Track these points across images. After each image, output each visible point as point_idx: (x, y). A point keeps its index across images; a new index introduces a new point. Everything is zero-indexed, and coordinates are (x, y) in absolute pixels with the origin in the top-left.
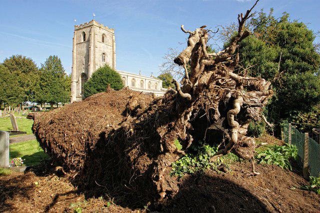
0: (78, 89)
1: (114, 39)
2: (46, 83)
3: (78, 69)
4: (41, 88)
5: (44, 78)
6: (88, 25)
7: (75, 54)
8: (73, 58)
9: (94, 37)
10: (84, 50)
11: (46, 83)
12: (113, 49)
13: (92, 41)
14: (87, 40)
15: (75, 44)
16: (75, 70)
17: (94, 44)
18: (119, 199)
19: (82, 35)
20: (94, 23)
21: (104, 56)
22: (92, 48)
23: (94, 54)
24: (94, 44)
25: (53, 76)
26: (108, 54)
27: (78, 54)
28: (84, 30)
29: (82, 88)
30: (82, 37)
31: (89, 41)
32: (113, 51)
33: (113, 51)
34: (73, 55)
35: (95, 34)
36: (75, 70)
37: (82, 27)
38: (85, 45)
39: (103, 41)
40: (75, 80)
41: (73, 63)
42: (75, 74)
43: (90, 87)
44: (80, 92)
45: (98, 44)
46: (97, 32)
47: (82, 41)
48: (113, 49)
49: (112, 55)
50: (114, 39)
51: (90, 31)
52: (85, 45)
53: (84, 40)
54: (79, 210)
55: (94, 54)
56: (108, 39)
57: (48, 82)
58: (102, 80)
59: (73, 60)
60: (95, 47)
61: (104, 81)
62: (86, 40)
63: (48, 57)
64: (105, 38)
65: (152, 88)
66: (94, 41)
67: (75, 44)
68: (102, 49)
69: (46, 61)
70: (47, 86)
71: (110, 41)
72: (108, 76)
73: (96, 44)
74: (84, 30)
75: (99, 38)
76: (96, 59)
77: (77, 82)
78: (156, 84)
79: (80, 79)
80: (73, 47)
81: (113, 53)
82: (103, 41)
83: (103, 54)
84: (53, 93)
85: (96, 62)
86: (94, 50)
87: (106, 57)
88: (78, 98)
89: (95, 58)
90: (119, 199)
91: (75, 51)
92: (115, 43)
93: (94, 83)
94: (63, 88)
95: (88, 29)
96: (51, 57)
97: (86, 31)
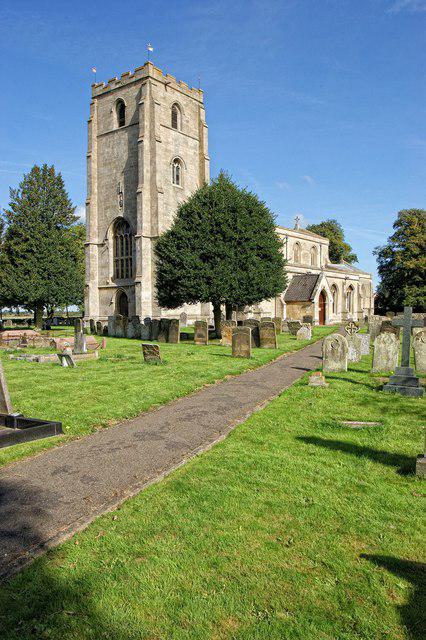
0: (104, 266)
1: (203, 118)
2: (24, 246)
3: (104, 206)
4: (13, 262)
5: (21, 231)
6: (134, 79)
7: (94, 166)
8: (90, 176)
9: (152, 113)
10: (122, 152)
11: (24, 246)
12: (201, 147)
13: (147, 123)
14: (130, 123)
15: (94, 136)
16: (95, 209)
17: (152, 131)
18: (31, 555)
19: (114, 111)
20: (152, 72)
21: (178, 168)
22: (146, 143)
23: (153, 162)
24: (152, 131)
25: (43, 226)
26: (186, 160)
27: (105, 163)
28: (120, 95)
29: (116, 261)
30: (115, 116)
31: (136, 124)
32: (201, 154)
33: (201, 154)
34: (89, 168)
35: (153, 104)
36: (95, 209)
37: (113, 87)
38: (125, 136)
39: (174, 125)
40: (96, 240)
41: (90, 192)
42: (95, 223)
43: (179, 248)
44: (111, 275)
45: (161, 132)
46: (161, 96)
47: (116, 126)
48: (201, 147)
49: (197, 164)
50: (203, 118)
51: (140, 96)
52: (125, 136)
53: (122, 123)
54: (324, 581)
55: (153, 162)
56: (188, 117)
57: (32, 241)
58: (218, 224)
59: (89, 184)
60: (154, 139)
61: (224, 228)
62: (128, 122)
63: (28, 172)
64: (179, 116)
65: (303, 262)
66: (152, 121)
67: (94, 136)
68: (171, 147)
69: (22, 180)
70: (29, 255)
71: (193, 126)
72: (234, 211)
73: (157, 132)
74: (120, 95)
75: (163, 115)
76: (158, 177)
77: (102, 245)
78: (296, 247)
79: (111, 235)
80: (90, 147)
81: (202, 160)
82: (174, 125)
83: (176, 161)
84: (47, 275)
85: (158, 184)
86: (153, 151)
87: (182, 171)
88: (105, 292)
89: (154, 172)
90: (31, 555)
91: (94, 156)
92: (205, 130)
93: (190, 234)
94: (70, 260)
95: (134, 91)
96: (35, 170)
97: (128, 96)
